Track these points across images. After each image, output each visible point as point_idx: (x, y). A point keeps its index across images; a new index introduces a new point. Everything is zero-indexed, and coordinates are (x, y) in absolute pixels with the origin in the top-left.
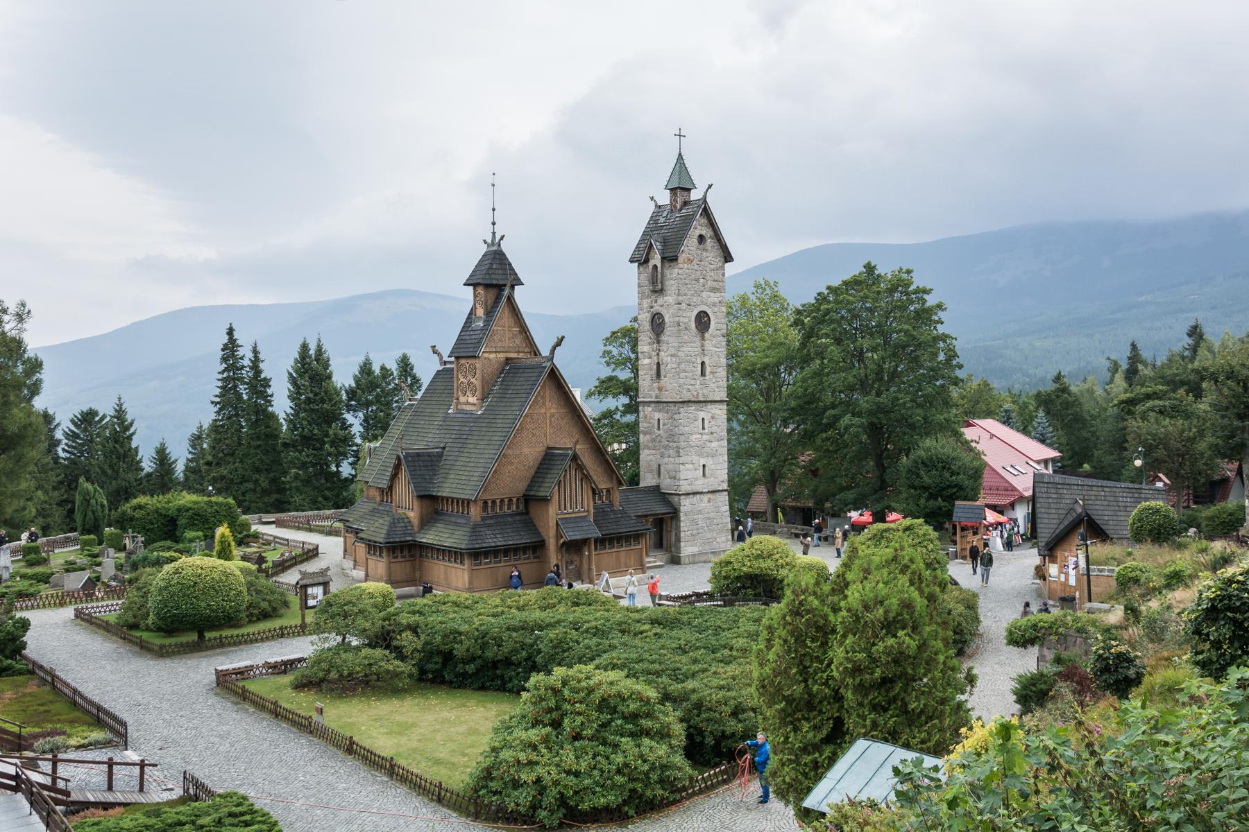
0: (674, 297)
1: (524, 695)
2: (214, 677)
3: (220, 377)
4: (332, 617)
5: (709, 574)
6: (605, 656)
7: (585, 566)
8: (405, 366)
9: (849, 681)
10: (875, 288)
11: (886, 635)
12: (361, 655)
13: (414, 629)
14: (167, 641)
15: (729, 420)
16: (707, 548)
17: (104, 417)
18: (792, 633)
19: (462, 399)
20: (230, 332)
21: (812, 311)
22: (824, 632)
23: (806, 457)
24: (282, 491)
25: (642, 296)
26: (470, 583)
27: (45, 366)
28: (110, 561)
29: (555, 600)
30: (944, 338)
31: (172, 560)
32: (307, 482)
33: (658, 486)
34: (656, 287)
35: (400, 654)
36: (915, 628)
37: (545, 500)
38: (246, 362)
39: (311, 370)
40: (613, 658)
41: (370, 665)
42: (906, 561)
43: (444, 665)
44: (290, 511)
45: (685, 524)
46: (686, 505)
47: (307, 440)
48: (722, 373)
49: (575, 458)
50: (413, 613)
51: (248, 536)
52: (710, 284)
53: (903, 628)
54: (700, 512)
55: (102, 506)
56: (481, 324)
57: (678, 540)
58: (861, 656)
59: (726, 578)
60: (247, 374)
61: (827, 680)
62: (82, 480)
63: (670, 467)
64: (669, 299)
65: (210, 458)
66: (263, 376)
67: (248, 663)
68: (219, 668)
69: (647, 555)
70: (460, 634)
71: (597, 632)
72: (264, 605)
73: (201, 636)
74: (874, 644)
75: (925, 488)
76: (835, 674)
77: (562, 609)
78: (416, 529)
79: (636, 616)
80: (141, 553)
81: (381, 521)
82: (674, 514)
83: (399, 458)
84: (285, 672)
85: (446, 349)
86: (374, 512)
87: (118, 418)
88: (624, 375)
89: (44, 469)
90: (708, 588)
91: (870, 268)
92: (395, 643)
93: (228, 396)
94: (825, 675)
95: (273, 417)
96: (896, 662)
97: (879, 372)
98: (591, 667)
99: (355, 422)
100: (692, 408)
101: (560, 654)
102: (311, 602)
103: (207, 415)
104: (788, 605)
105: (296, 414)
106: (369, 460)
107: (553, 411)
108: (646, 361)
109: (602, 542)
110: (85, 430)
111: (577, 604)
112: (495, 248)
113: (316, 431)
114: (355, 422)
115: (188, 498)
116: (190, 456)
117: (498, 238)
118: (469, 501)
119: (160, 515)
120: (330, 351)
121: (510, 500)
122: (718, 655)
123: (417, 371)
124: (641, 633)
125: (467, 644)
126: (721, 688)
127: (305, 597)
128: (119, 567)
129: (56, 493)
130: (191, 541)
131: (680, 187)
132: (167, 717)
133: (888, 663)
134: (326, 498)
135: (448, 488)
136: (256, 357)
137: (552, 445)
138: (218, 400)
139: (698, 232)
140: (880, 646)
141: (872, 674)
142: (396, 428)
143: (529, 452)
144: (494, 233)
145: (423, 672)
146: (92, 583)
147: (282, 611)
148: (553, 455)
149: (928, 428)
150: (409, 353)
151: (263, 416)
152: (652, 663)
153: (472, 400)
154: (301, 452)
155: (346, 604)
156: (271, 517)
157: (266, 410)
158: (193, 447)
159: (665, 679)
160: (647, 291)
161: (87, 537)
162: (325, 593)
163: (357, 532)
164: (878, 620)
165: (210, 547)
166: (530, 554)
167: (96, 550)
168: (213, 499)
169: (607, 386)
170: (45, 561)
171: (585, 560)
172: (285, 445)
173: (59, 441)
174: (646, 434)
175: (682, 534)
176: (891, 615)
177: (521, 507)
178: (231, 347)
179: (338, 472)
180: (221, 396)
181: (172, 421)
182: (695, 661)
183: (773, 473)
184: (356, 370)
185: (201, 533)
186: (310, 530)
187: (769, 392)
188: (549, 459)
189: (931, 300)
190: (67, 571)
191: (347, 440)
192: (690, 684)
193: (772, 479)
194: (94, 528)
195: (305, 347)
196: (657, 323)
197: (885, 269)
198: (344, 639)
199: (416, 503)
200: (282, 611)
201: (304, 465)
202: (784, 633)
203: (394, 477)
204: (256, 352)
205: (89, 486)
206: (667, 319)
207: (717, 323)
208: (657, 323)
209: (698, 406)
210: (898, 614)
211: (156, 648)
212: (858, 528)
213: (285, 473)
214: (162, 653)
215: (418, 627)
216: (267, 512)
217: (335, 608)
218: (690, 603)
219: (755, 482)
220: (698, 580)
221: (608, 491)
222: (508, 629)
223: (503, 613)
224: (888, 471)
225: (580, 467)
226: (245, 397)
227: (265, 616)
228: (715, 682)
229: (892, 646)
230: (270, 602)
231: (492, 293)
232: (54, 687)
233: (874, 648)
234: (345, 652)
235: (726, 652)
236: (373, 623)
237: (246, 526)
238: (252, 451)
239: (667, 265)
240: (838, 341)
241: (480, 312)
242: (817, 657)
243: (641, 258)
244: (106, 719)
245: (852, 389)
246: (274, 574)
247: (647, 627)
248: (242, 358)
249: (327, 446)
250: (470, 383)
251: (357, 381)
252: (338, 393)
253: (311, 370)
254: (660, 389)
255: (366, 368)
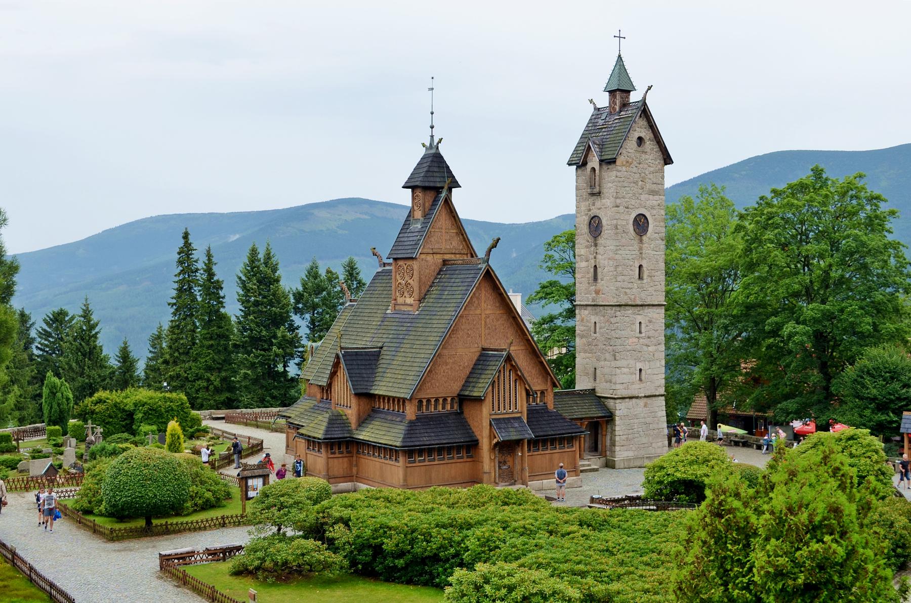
0: (612, 199)
1: (448, 590)
2: (158, 562)
3: (177, 279)
4: (268, 508)
5: (643, 480)
6: (530, 555)
7: (518, 467)
8: (351, 271)
9: (771, 585)
10: (824, 192)
11: (812, 539)
12: (297, 546)
13: (346, 522)
14: (117, 526)
15: (667, 326)
16: (642, 453)
17: (73, 318)
18: (711, 534)
19: (400, 300)
20: (186, 236)
21: (755, 215)
22: (747, 534)
23: (746, 366)
24: (231, 388)
25: (579, 198)
26: (405, 480)
27: (22, 269)
28: (71, 451)
29: (485, 499)
30: (895, 246)
31: (124, 450)
32: (255, 381)
33: (594, 390)
34: (592, 190)
35: (331, 543)
36: (843, 534)
37: (479, 400)
38: (200, 265)
39: (261, 277)
40: (538, 558)
41: (303, 555)
42: (837, 464)
43: (374, 557)
44: (238, 408)
45: (620, 426)
46: (621, 410)
47: (255, 341)
48: (661, 277)
49: (509, 359)
50: (346, 507)
51: (198, 431)
52: (649, 186)
53: (831, 534)
54: (636, 417)
55: (68, 399)
56: (419, 226)
57: (613, 444)
58: (782, 561)
59: (660, 482)
60: (201, 276)
61: (748, 584)
62: (49, 374)
63: (606, 370)
64: (607, 201)
65: (167, 357)
66: (215, 278)
67: (188, 549)
68: (163, 553)
69: (581, 458)
70: (390, 529)
71: (526, 532)
72: (208, 495)
73: (149, 523)
74: (799, 549)
75: (874, 399)
76: (756, 578)
77: (491, 507)
78: (353, 426)
79: (566, 517)
80: (100, 444)
81: (320, 418)
82: (610, 418)
83: (337, 357)
84: (224, 559)
85: (385, 252)
86: (315, 409)
87: (84, 317)
88: (565, 280)
89: (19, 365)
90: (642, 493)
91: (818, 173)
92: (327, 534)
93: (184, 303)
94: (745, 580)
95: (223, 318)
96: (821, 567)
97: (825, 281)
98: (515, 565)
99: (302, 323)
100: (630, 311)
101: (488, 550)
102: (251, 494)
103: (166, 318)
104: (707, 506)
105: (246, 315)
106: (312, 363)
107: (488, 312)
108: (584, 264)
109: (534, 444)
110: (57, 329)
111: (506, 504)
112: (433, 151)
113: (264, 333)
114: (302, 323)
115: (143, 394)
116: (150, 355)
117: (436, 141)
118: (404, 400)
119: (119, 409)
120: (278, 258)
121: (445, 400)
122: (645, 559)
123: (361, 276)
124: (569, 534)
125: (396, 538)
126: (646, 591)
127: (246, 489)
128: (80, 457)
129: (30, 388)
130: (146, 434)
131: (620, 90)
132: (113, 596)
133: (813, 569)
134: (274, 397)
135: (384, 386)
136: (209, 260)
137: (486, 346)
138: (174, 301)
139: (637, 135)
140: (805, 551)
141: (795, 580)
142: (336, 328)
143: (465, 354)
144: (432, 136)
145: (354, 563)
146: (53, 470)
147: (224, 503)
148: (488, 356)
149: (875, 337)
150: (356, 259)
151: (216, 317)
152: (579, 563)
153: (409, 301)
154: (249, 353)
155: (282, 496)
156: (221, 413)
157: (218, 311)
158: (153, 346)
159: (589, 580)
160: (585, 195)
161: (53, 427)
162: (264, 484)
163: (298, 427)
164: (803, 524)
165: (162, 440)
166: (463, 453)
167: (60, 440)
168: (168, 395)
169: (548, 291)
170: (15, 449)
171: (518, 461)
172: (235, 346)
173: (33, 340)
174: (582, 337)
175: (617, 438)
176: (818, 519)
177: (456, 406)
178: (186, 250)
179: (285, 372)
180: (178, 297)
181: (134, 323)
182: (622, 563)
183: (713, 380)
184: (303, 275)
185: (154, 427)
186: (257, 427)
187: (712, 299)
188: (484, 357)
189: (884, 207)
190: (34, 458)
191: (293, 342)
192: (615, 586)
193: (712, 387)
194: (60, 419)
195: (254, 252)
196: (595, 226)
197: (837, 177)
198: (279, 530)
199: (354, 402)
200: (224, 503)
201: (253, 366)
202: (703, 535)
203: (333, 374)
204: (209, 256)
205: (56, 380)
206: (604, 222)
207: (655, 227)
208: (595, 226)
209: (636, 309)
210: (825, 519)
211: (107, 532)
212: (797, 437)
213: (235, 372)
214: (112, 537)
215: (350, 520)
216: (218, 409)
217: (271, 500)
218: (622, 506)
219: (695, 389)
220: (634, 484)
221: (542, 393)
222: (437, 526)
223: (433, 509)
224: (834, 381)
225: (515, 368)
226: (199, 299)
227: (208, 506)
228: (639, 585)
229: (817, 551)
230: (214, 492)
231: (430, 196)
232: (14, 564)
233: (798, 554)
234: (280, 541)
235: (655, 556)
236: (311, 514)
237: (196, 421)
238: (205, 351)
239: (605, 167)
240: (784, 246)
241: (418, 214)
242: (739, 560)
243: (580, 162)
244: (59, 597)
245: (796, 295)
246: (220, 467)
247: (575, 528)
248: (196, 261)
249: (274, 348)
250: (407, 284)
251: (304, 285)
252: (286, 297)
253: (261, 277)
254: (597, 292)
255: (313, 273)
